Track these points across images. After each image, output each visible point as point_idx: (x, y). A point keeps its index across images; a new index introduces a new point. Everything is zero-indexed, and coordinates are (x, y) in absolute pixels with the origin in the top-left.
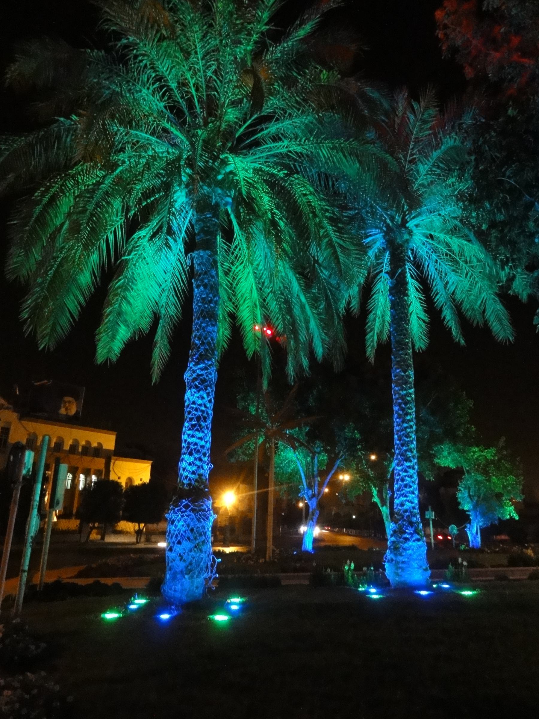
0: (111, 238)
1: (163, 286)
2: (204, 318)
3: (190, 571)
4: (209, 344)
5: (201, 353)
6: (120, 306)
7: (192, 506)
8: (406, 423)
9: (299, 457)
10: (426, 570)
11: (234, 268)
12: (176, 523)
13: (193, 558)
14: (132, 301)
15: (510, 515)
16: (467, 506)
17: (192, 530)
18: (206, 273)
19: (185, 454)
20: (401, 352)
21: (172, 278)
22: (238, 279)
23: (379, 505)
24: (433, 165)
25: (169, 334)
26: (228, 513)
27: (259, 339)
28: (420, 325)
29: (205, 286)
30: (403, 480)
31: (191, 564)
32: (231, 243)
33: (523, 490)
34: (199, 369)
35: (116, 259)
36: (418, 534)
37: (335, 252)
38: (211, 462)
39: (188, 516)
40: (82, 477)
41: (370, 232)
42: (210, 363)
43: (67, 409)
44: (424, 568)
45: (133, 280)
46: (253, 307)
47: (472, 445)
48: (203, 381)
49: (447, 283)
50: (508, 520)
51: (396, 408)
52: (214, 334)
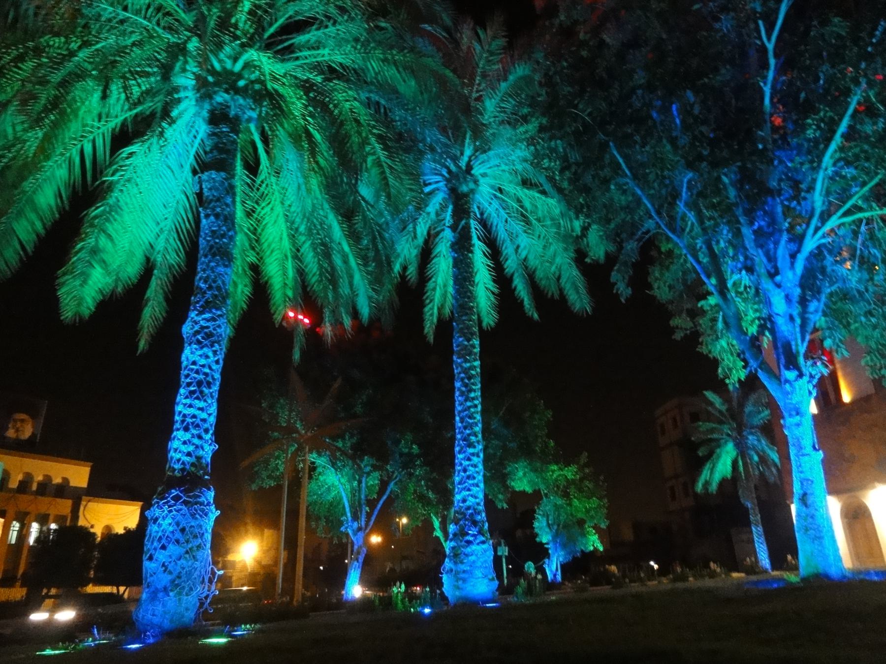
0: (88, 148)
1: (162, 225)
2: (214, 255)
3: (177, 585)
4: (219, 289)
5: (206, 300)
6: (97, 240)
7: (185, 498)
8: (470, 401)
9: (343, 480)
10: (493, 579)
11: (259, 209)
12: (160, 521)
13: (183, 568)
14: (114, 235)
15: (593, 546)
16: (545, 538)
17: (183, 530)
18: (218, 200)
19: (178, 430)
20: (464, 318)
21: (175, 215)
22: (264, 223)
23: (442, 540)
24: (502, 100)
25: (166, 289)
26: (247, 570)
27: (289, 299)
28: (489, 297)
29: (217, 216)
30: (465, 471)
31: (179, 577)
32: (255, 176)
33: (607, 514)
34: (203, 319)
35: (95, 178)
36: (483, 535)
37: (383, 173)
38: (216, 442)
39: (178, 511)
40: (35, 527)
41: (430, 179)
42: (219, 313)
43: (17, 431)
44: (490, 577)
45: (116, 208)
46: (283, 260)
47: (550, 463)
48: (209, 336)
49: (518, 247)
50: (591, 552)
51: (458, 384)
52: (226, 276)
